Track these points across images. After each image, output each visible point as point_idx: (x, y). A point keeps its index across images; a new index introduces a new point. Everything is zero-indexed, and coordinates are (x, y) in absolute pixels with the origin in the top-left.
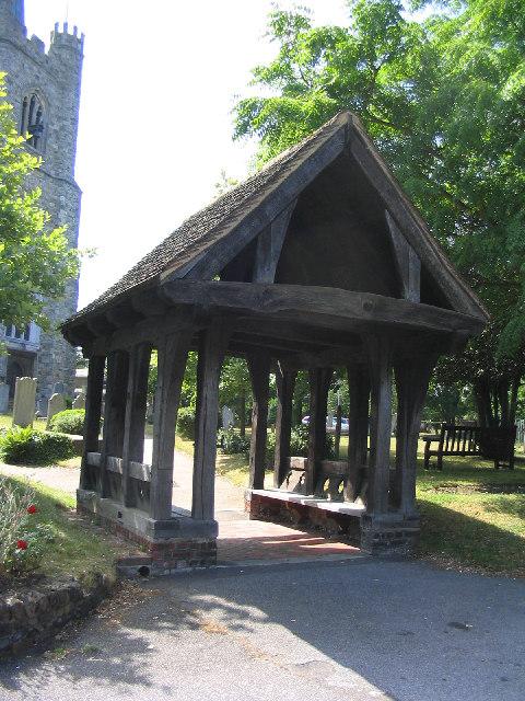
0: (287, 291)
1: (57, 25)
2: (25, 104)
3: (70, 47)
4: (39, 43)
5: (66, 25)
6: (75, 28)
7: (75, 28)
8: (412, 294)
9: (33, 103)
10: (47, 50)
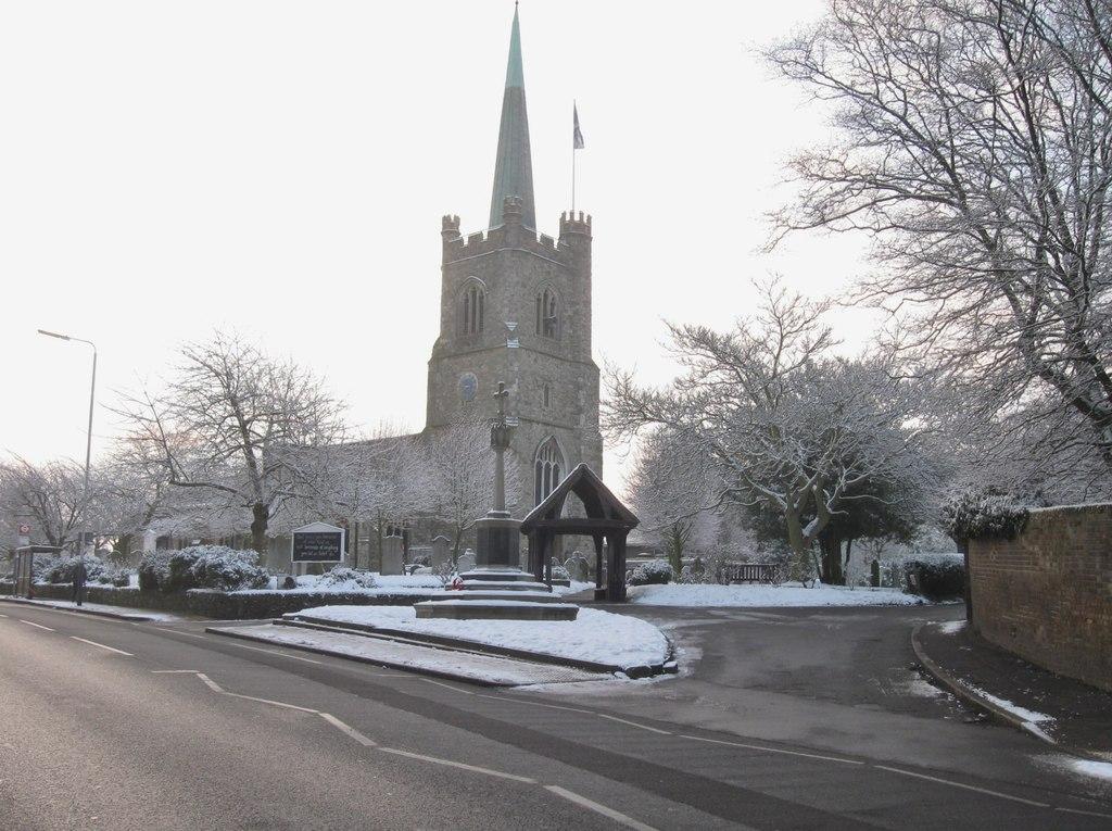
0: (523, 557)
1: (564, 214)
2: (539, 300)
3: (577, 233)
4: (547, 241)
5: (572, 214)
6: (581, 214)
7: (581, 214)
8: (608, 518)
9: (546, 296)
10: (556, 243)
